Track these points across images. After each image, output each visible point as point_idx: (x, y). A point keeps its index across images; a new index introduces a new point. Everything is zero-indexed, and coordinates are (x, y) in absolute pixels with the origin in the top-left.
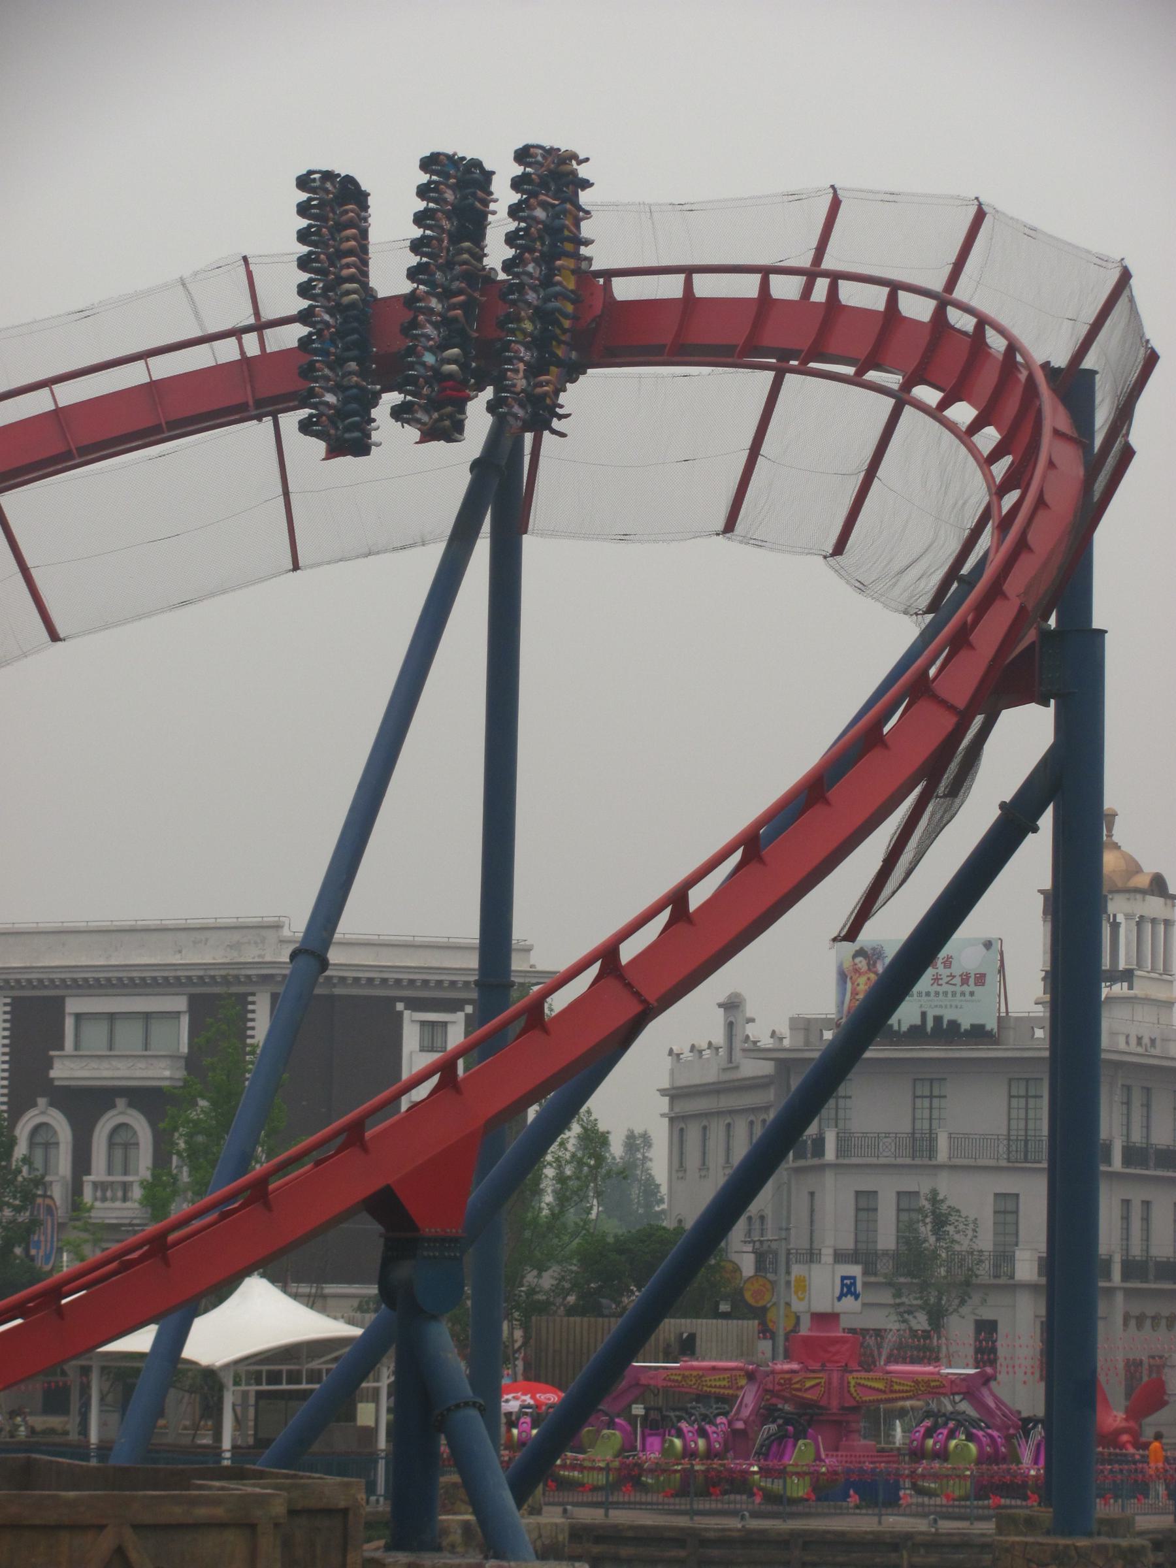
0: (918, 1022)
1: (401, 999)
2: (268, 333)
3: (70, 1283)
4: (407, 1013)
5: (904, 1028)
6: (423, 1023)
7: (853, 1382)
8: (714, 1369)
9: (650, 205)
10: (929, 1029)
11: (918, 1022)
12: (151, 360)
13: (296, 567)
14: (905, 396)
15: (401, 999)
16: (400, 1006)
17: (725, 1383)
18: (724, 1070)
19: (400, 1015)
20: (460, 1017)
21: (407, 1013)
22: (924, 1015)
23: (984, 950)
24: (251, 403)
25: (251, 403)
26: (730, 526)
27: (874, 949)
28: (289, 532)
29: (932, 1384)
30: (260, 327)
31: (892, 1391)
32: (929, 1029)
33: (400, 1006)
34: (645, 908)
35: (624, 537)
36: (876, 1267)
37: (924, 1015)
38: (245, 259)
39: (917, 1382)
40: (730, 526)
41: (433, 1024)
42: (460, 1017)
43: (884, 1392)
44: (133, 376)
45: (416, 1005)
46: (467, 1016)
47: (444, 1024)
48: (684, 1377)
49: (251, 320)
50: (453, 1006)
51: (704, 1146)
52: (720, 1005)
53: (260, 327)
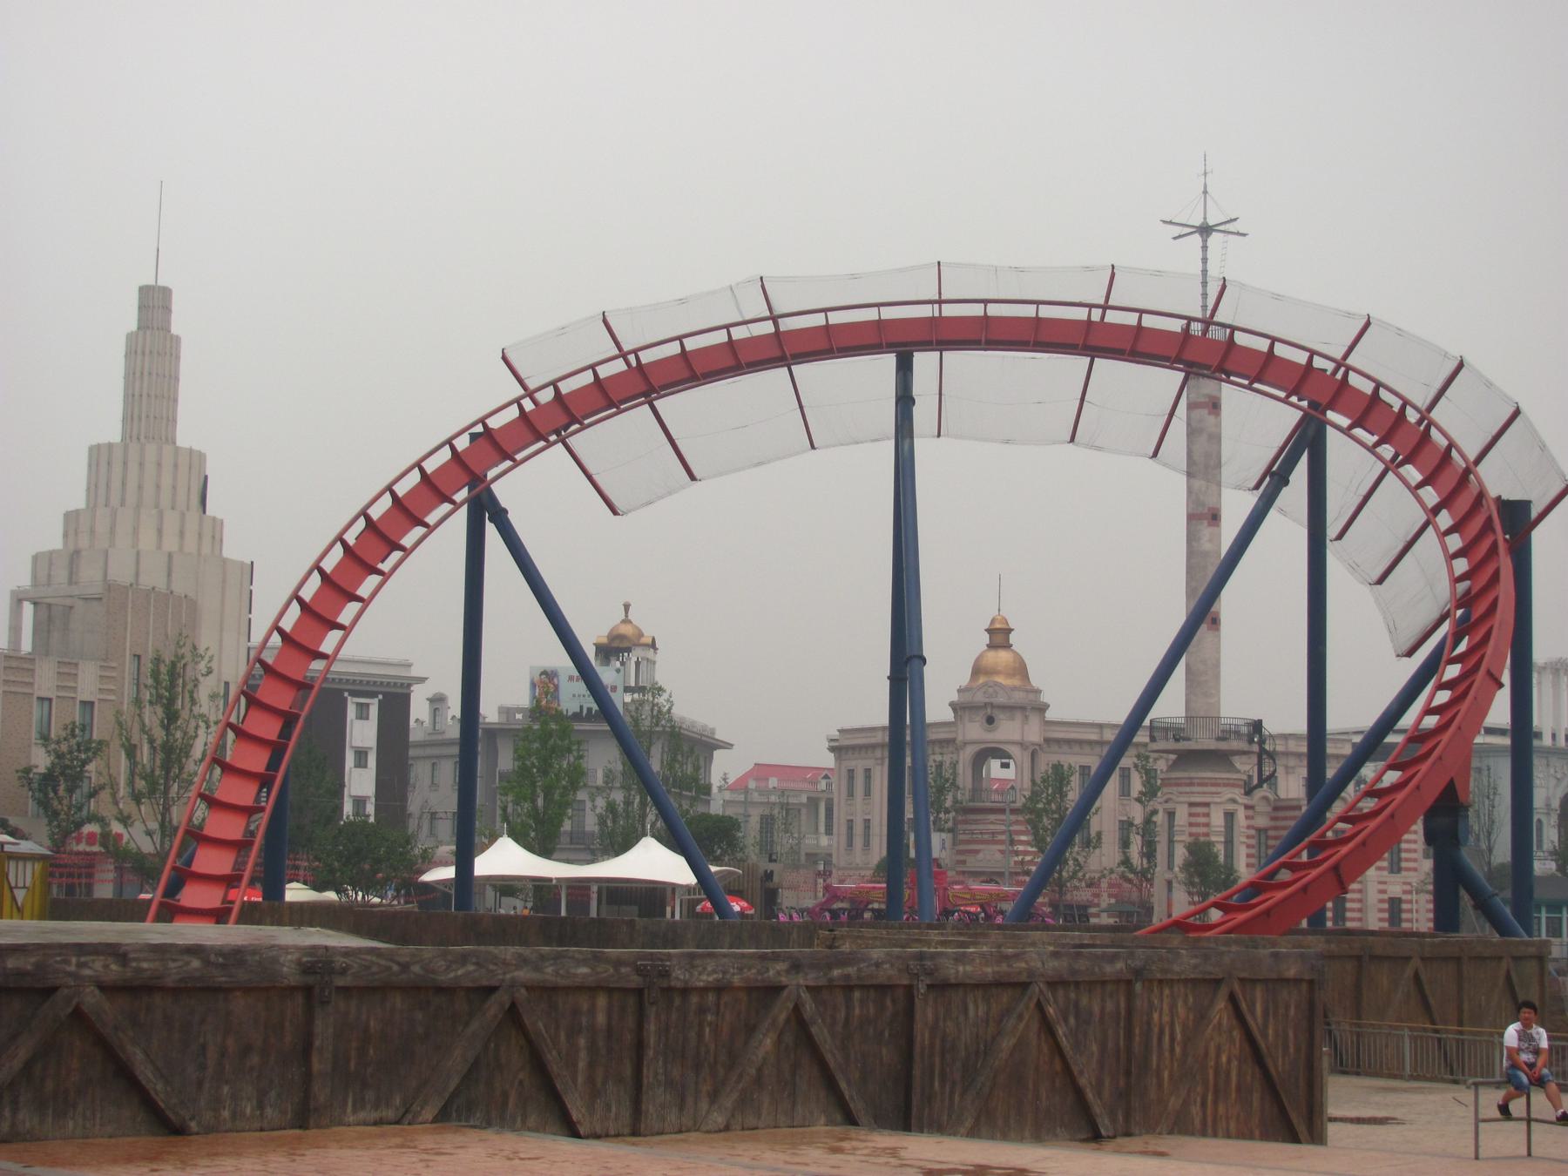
0: (578, 710)
1: (346, 690)
2: (943, 306)
3: (978, 844)
4: (349, 698)
5: (570, 714)
6: (358, 704)
7: (951, 895)
8: (874, 888)
9: (996, 267)
10: (584, 714)
11: (578, 710)
12: (881, 308)
13: (939, 435)
14: (529, 392)
15: (346, 690)
16: (346, 694)
17: (881, 895)
18: (429, 734)
19: (346, 699)
20: (376, 701)
21: (349, 698)
22: (581, 707)
23: (227, 680)
24: (983, 339)
25: (983, 339)
26: (1072, 439)
27: (552, 671)
28: (662, 420)
29: (1001, 895)
30: (940, 302)
31: (974, 900)
32: (584, 714)
33: (346, 694)
34: (1173, 639)
35: (1007, 442)
36: (772, 837)
37: (581, 707)
38: (939, 263)
39: (991, 895)
40: (1072, 439)
41: (362, 704)
42: (376, 701)
43: (970, 900)
44: (870, 315)
45: (354, 694)
46: (379, 700)
47: (368, 705)
48: (860, 892)
49: (937, 298)
50: (372, 695)
51: (433, 774)
52: (428, 699)
53: (940, 302)
